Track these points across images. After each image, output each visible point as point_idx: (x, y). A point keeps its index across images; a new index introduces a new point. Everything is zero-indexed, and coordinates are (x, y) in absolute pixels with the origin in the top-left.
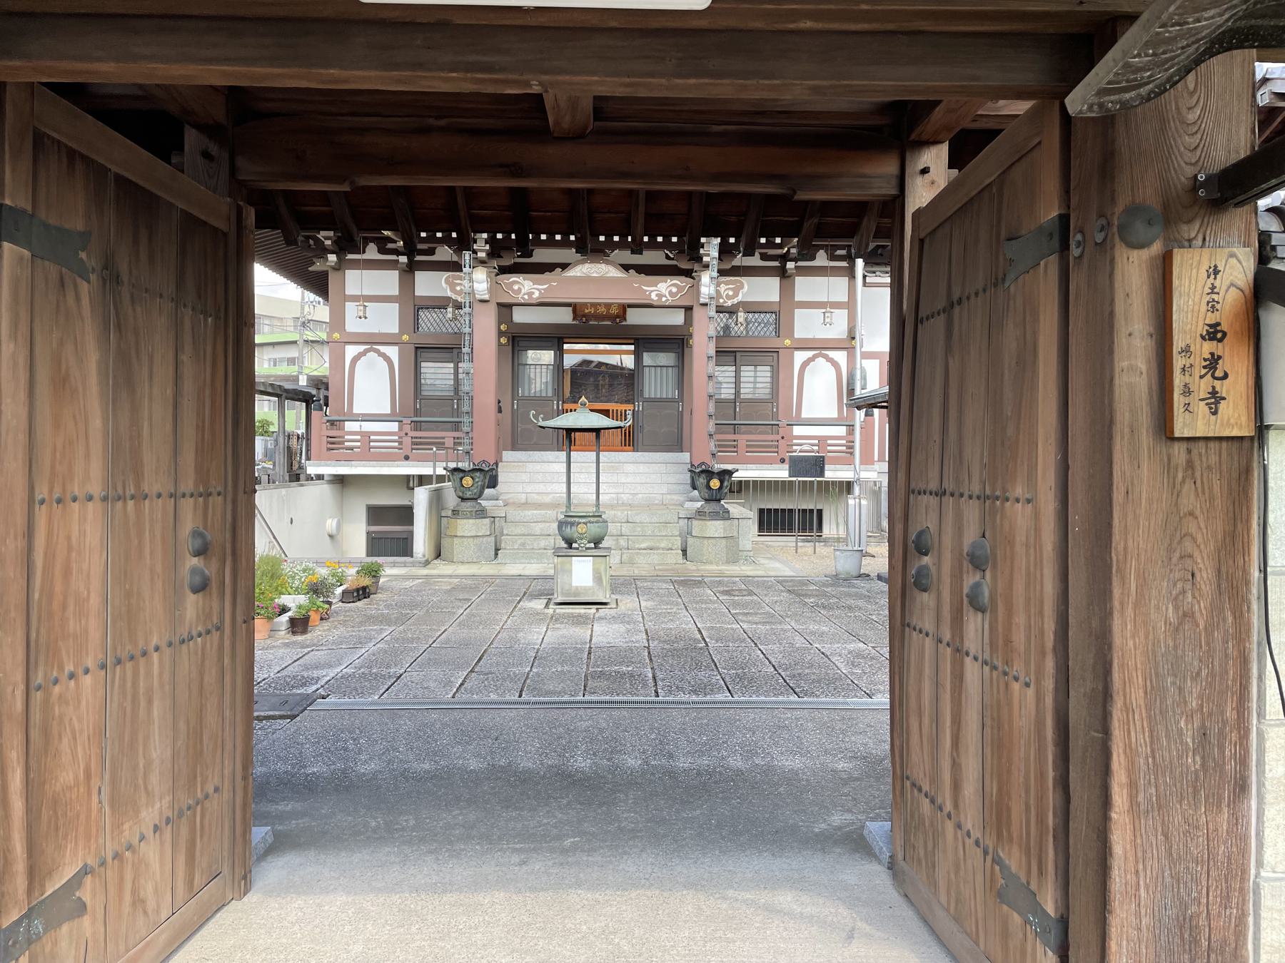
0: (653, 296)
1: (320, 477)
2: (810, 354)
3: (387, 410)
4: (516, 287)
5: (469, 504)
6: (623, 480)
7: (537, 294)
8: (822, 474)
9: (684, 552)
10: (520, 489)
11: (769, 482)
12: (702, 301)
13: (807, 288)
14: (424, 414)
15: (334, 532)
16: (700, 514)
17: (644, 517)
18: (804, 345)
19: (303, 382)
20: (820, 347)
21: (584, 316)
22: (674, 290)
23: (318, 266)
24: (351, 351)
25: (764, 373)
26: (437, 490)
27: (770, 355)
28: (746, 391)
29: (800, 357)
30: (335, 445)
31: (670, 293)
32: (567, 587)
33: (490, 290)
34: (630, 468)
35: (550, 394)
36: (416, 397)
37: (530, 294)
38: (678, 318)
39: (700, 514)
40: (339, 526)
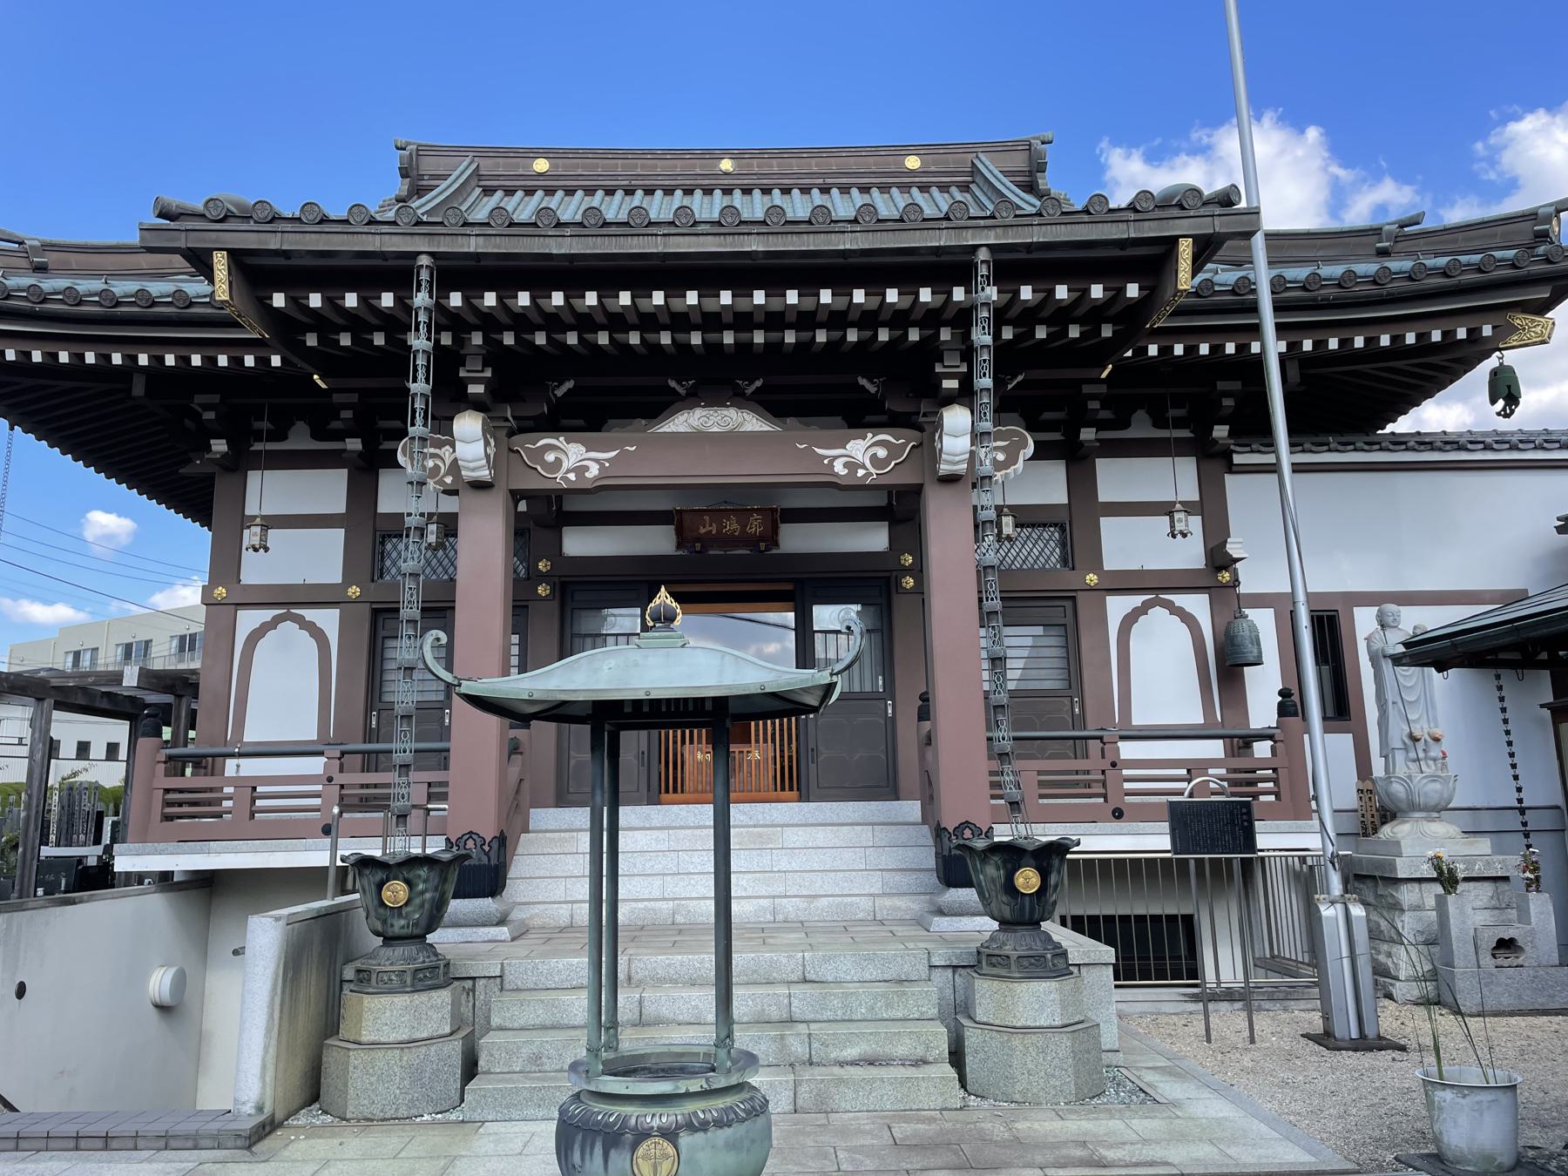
0: (839, 467)
1: (140, 878)
2: (1137, 600)
3: (308, 731)
4: (550, 457)
5: (399, 951)
6: (784, 866)
7: (594, 471)
9: (957, 1057)
10: (559, 894)
11: (1104, 863)
12: (944, 469)
13: (1117, 479)
14: (374, 734)
16: (986, 961)
17: (844, 966)
18: (1126, 583)
19: (131, 678)
20: (1156, 586)
21: (699, 539)
22: (882, 453)
23: (197, 466)
24: (248, 620)
26: (332, 922)
29: (1118, 607)
30: (188, 809)
31: (874, 458)
33: (494, 463)
34: (795, 837)
36: (370, 705)
37: (580, 470)
38: (874, 539)
39: (986, 961)
40: (180, 982)
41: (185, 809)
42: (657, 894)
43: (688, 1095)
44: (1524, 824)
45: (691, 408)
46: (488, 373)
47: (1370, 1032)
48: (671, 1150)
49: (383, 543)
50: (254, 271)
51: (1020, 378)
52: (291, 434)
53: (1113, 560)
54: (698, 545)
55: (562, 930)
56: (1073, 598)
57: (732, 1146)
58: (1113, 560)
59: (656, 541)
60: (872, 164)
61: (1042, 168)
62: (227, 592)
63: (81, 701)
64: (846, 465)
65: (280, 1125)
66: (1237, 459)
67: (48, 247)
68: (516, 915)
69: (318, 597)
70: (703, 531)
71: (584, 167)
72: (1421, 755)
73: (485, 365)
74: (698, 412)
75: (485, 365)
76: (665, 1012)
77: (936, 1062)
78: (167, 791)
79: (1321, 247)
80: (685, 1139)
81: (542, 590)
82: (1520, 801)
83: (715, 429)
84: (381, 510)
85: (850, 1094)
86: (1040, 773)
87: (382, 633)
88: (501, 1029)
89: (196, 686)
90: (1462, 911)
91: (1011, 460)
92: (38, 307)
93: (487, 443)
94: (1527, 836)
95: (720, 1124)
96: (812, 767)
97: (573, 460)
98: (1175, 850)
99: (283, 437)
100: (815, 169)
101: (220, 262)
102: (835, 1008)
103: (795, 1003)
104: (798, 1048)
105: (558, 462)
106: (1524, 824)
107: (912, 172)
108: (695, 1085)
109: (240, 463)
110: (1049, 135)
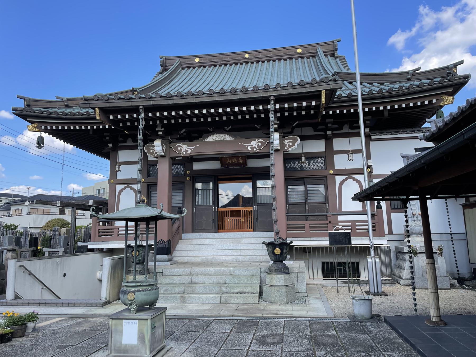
4: (179, 149)
6: (242, 248)
7: (189, 152)
8: (350, 243)
11: (305, 248)
15: (100, 278)
20: (350, 173)
21: (227, 164)
22: (260, 144)
24: (119, 188)
25: (321, 188)
27: (323, 179)
28: (312, 199)
29: (339, 179)
31: (258, 146)
32: (118, 345)
34: (246, 241)
35: (211, 204)
37: (186, 151)
41: (106, 234)
42: (210, 255)
43: (138, 286)
44: (452, 238)
45: (213, 135)
46: (163, 129)
47: (380, 291)
48: (134, 295)
49: (150, 168)
50: (105, 111)
51: (296, 123)
52: (127, 141)
53: (338, 166)
54: (226, 166)
55: (185, 263)
56: (326, 177)
57: (145, 295)
58: (338, 166)
59: (216, 165)
60: (288, 52)
61: (336, 50)
62: (114, 181)
63: (83, 208)
64: (251, 148)
65: (111, 303)
66: (373, 137)
67: (68, 100)
68: (175, 259)
69: (134, 182)
70: (227, 162)
71: (209, 59)
72: (415, 219)
73: (162, 127)
74: (215, 136)
75: (162, 127)
76: (197, 281)
77: (256, 293)
78: (99, 229)
79: (394, 77)
80: (136, 293)
81: (188, 179)
82: (451, 231)
83: (219, 140)
84: (149, 159)
85: (233, 299)
86: (310, 224)
87: (150, 190)
88: (161, 284)
89: (107, 204)
90: (418, 261)
91: (294, 145)
92: (65, 117)
93: (163, 146)
94: (452, 241)
95: (143, 291)
96: (256, 223)
97: (185, 149)
98: (330, 244)
99: (125, 142)
100: (272, 55)
101: (97, 109)
102: (235, 281)
103: (226, 279)
104: (224, 289)
105: (181, 149)
106: (452, 238)
107: (299, 54)
108: (139, 284)
109: (116, 149)
110: (339, 39)
